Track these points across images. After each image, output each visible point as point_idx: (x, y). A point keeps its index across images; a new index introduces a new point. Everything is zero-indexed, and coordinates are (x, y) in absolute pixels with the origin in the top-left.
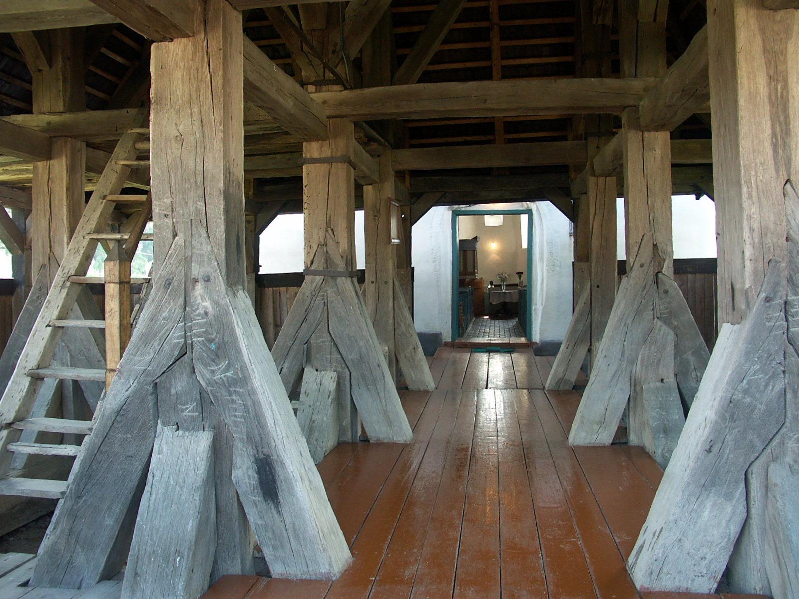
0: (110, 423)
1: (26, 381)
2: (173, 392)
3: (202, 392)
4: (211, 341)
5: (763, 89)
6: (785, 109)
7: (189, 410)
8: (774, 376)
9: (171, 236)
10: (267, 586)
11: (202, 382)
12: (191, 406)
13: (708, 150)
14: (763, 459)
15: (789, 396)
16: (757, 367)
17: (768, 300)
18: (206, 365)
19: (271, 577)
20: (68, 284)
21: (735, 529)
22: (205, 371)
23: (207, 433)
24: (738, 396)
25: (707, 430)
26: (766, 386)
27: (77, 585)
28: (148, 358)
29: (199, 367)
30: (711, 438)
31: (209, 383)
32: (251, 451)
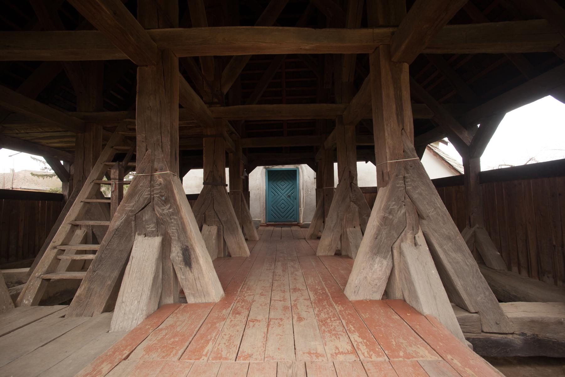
0: (112, 235)
1: (69, 227)
2: (144, 219)
3: (157, 219)
4: (162, 196)
5: (392, 92)
6: (401, 100)
7: (151, 227)
8: (401, 207)
9: (145, 150)
10: (186, 307)
11: (158, 215)
12: (152, 226)
13: (372, 140)
14: (398, 241)
15: (407, 215)
16: (394, 203)
17: (397, 176)
18: (160, 207)
19: (187, 303)
20: (93, 184)
21: (388, 272)
22: (159, 210)
23: (159, 237)
24: (387, 215)
25: (375, 230)
26: (398, 211)
27: (91, 315)
28: (132, 204)
29: (157, 208)
30: (377, 232)
31: (161, 215)
32: (180, 244)
